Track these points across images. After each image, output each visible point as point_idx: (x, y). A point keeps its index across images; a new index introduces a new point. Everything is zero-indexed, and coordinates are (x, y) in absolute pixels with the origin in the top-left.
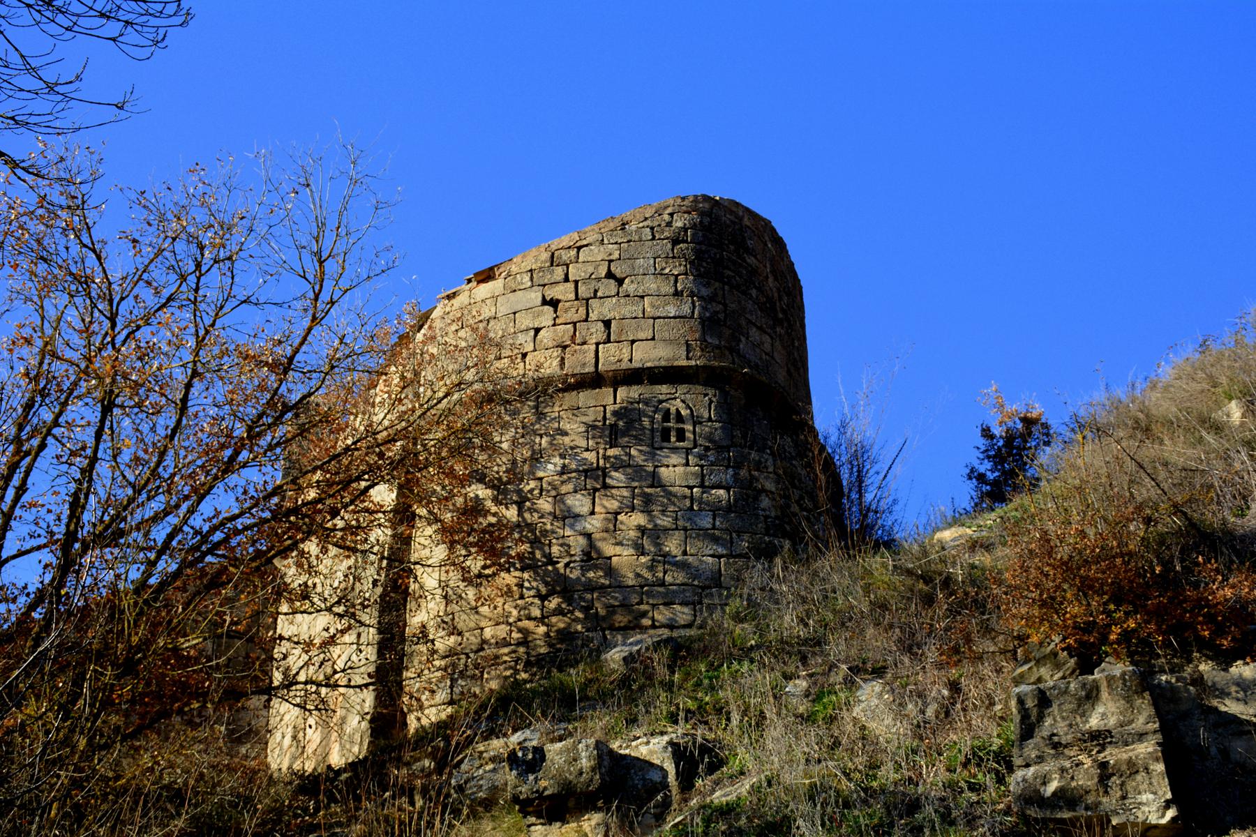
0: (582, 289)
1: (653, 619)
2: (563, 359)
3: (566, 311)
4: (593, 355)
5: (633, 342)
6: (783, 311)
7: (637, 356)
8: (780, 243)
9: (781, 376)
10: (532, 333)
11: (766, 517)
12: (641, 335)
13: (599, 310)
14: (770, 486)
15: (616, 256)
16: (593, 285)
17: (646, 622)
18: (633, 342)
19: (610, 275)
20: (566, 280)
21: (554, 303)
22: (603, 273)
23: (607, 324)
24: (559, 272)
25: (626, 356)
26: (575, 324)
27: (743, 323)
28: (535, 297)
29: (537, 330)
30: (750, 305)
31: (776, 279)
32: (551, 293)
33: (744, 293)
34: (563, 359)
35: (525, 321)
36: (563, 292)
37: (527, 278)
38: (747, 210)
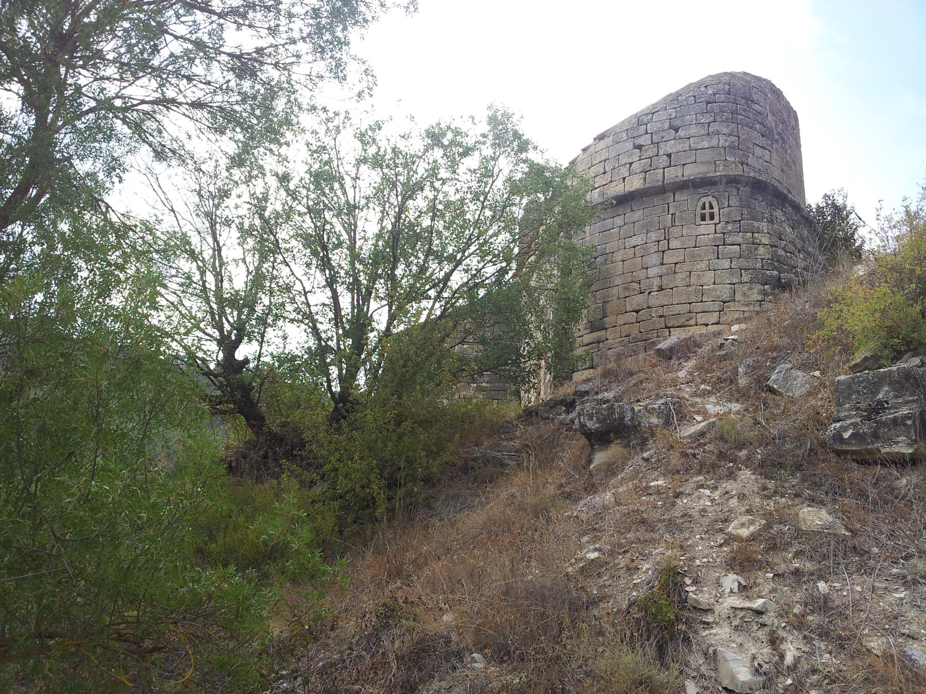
0: (655, 137)
1: (390, 160)
2: (645, 179)
3: (646, 151)
4: (661, 175)
5: (684, 165)
6: (780, 134)
7: (687, 173)
8: (778, 93)
9: (777, 174)
10: (628, 166)
11: (762, 259)
12: (688, 161)
13: (666, 148)
14: (765, 241)
15: (674, 115)
16: (662, 134)
17: (693, 322)
18: (684, 165)
19: (671, 127)
20: (647, 133)
21: (639, 147)
22: (666, 126)
23: (669, 156)
24: (643, 128)
25: (680, 174)
26: (669, 249)
27: (750, 145)
28: (629, 145)
29: (631, 164)
30: (755, 134)
31: (773, 115)
32: (639, 141)
33: (751, 128)
34: (645, 179)
35: (625, 160)
36: (645, 140)
37: (624, 135)
38: (755, 77)
